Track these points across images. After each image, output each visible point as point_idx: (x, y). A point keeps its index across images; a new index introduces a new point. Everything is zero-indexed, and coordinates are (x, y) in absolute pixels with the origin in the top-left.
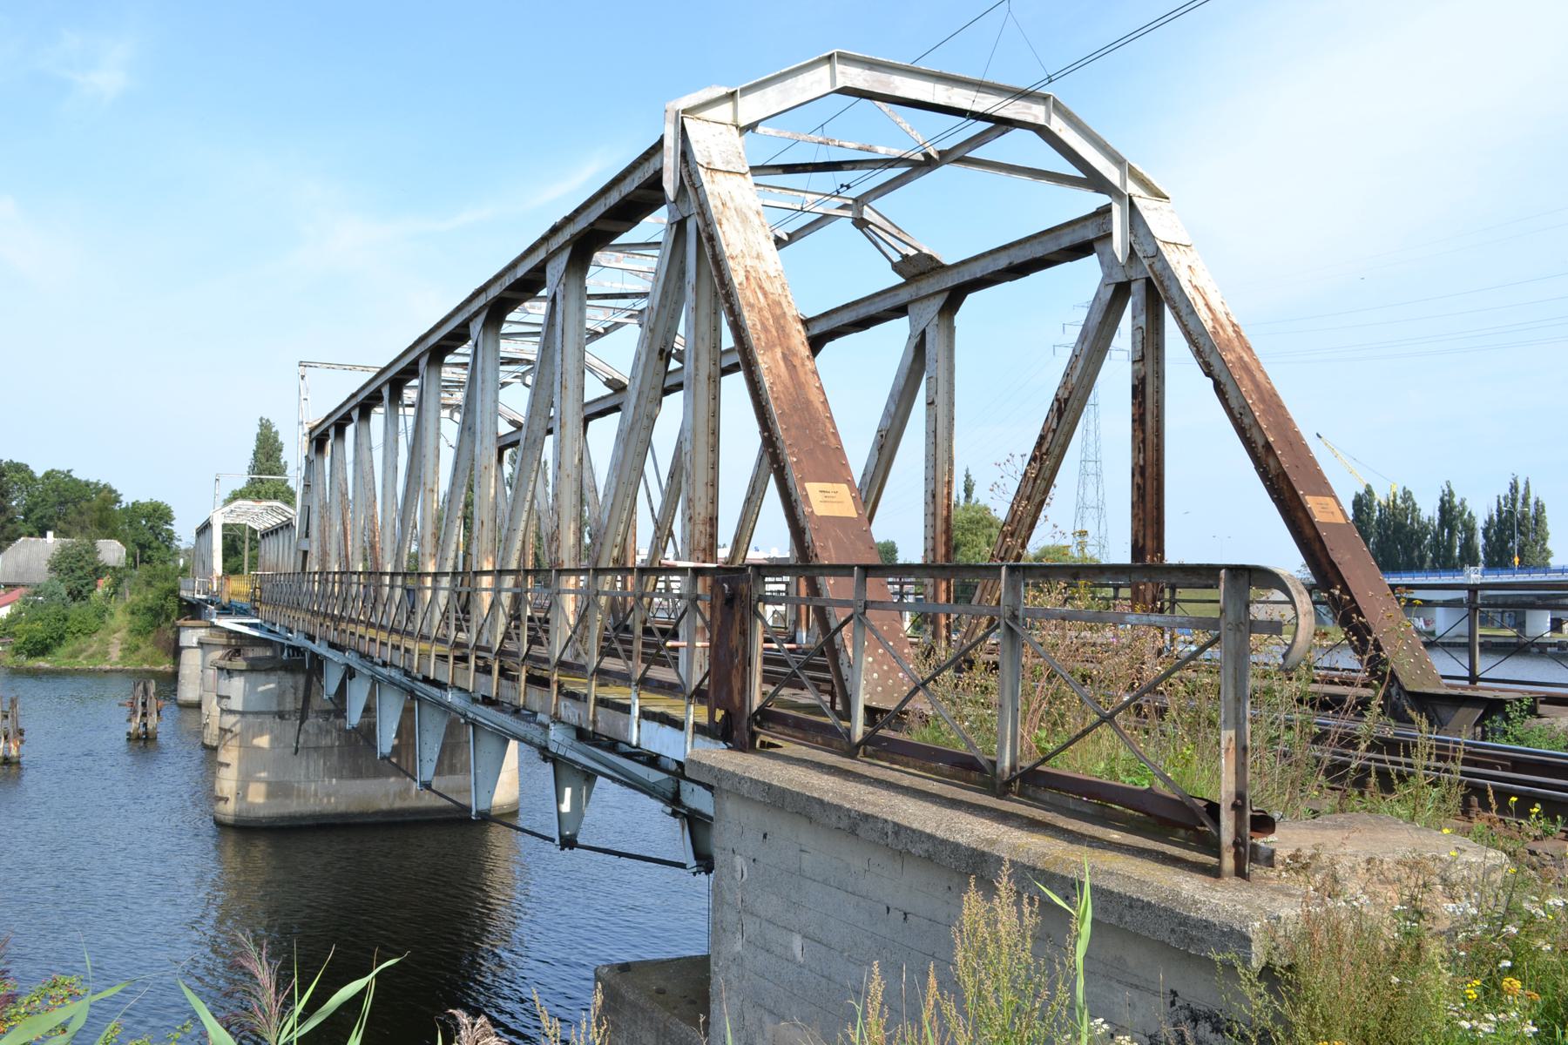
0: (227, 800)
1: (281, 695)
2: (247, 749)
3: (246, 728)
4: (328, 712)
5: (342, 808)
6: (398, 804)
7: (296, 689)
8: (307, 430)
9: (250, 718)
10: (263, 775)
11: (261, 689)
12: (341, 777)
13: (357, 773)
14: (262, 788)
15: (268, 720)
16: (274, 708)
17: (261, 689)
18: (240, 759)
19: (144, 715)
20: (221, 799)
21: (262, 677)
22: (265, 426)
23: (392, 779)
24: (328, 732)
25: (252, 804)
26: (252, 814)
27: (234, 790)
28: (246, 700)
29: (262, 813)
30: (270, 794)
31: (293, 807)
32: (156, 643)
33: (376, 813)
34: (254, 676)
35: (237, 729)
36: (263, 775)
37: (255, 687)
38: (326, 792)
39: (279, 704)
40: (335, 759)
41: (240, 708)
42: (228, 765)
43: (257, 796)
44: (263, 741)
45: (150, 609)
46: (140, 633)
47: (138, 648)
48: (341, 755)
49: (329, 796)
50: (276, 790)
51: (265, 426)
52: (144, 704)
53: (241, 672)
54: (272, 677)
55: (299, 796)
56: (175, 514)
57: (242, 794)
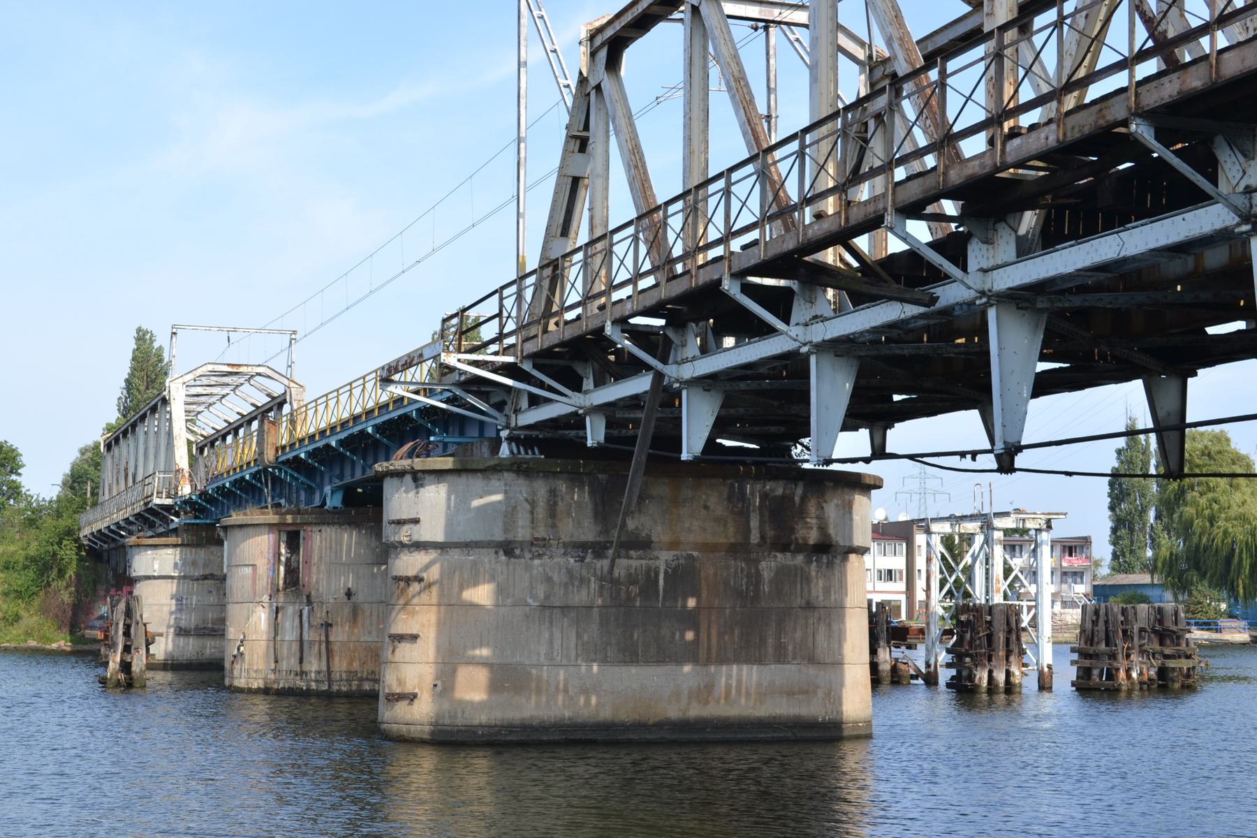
0: (412, 697)
1: (508, 513)
2: (453, 608)
3: (448, 574)
4: (583, 546)
5: (606, 714)
6: (696, 711)
7: (533, 504)
8: (584, 35)
9: (455, 555)
10: (485, 652)
11: (476, 503)
12: (604, 661)
13: (630, 656)
14: (481, 676)
15: (487, 558)
16: (499, 536)
17: (476, 503)
18: (441, 626)
19: (127, 649)
20: (400, 697)
21: (477, 482)
22: (143, 338)
23: (687, 668)
24: (583, 581)
25: (461, 702)
26: (460, 721)
27: (429, 679)
28: (450, 524)
29: (482, 718)
30: (495, 687)
31: (528, 708)
32: (44, 611)
33: (660, 725)
34: (462, 481)
35: (434, 573)
36: (485, 652)
37: (463, 501)
38: (586, 685)
39: (506, 530)
40: (593, 630)
41: (440, 538)
42: (414, 638)
43: (473, 688)
44: (482, 594)
45: (33, 560)
46: (19, 595)
47: (17, 618)
48: (604, 622)
49: (586, 691)
50: (505, 678)
51: (143, 338)
52: (127, 633)
53: (439, 474)
54: (495, 482)
55: (539, 691)
56: (24, 459)
57: (445, 683)
